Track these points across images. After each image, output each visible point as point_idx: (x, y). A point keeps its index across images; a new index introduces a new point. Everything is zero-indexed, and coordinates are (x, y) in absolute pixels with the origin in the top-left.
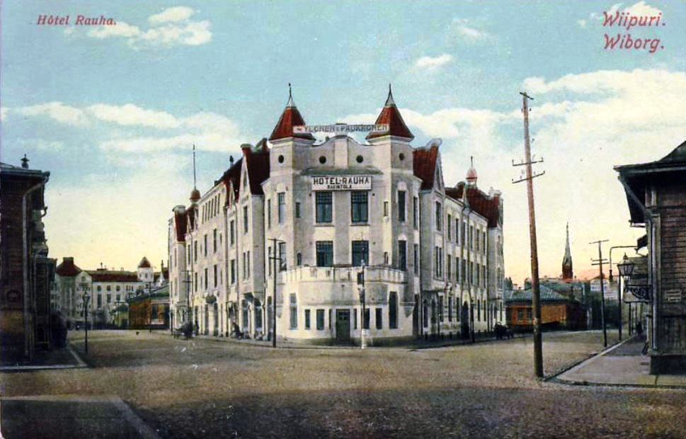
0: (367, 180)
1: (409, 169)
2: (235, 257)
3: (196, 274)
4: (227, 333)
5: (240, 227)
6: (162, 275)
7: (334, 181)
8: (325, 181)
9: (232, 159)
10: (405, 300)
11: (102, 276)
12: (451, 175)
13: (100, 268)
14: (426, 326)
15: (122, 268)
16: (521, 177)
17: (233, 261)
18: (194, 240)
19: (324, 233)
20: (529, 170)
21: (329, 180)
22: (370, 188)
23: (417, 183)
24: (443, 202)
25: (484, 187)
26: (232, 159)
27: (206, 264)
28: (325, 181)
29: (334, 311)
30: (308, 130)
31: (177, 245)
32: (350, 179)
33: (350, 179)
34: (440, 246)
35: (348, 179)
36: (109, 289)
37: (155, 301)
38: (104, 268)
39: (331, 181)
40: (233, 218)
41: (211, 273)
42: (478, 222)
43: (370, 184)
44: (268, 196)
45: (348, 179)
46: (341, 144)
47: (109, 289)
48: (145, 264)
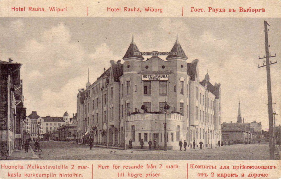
0: (167, 76)
1: (185, 72)
2: (106, 110)
3: (89, 117)
4: (102, 143)
5: (109, 97)
6: (73, 118)
7: (152, 76)
8: (148, 76)
9: (105, 69)
10: (183, 129)
11: (48, 119)
12: (201, 76)
13: (47, 116)
14: (191, 141)
15: (53, 116)
16: (263, 64)
17: (105, 111)
18: (88, 103)
19: (146, 99)
20: (268, 61)
21: (150, 76)
22: (168, 80)
23: (188, 77)
24: (199, 87)
25: (213, 82)
26: (105, 69)
27: (93, 113)
28: (148, 76)
29: (152, 134)
30: (141, 54)
31: (81, 106)
32: (159, 75)
33: (159, 75)
34: (197, 106)
35: (160, 76)
36: (51, 124)
37: (70, 129)
38: (49, 116)
39: (151, 76)
40: (106, 93)
41: (95, 117)
42: (211, 96)
43: (168, 78)
44: (122, 83)
45: (158, 75)
46: (155, 61)
47: (51, 124)
48: (66, 114)
